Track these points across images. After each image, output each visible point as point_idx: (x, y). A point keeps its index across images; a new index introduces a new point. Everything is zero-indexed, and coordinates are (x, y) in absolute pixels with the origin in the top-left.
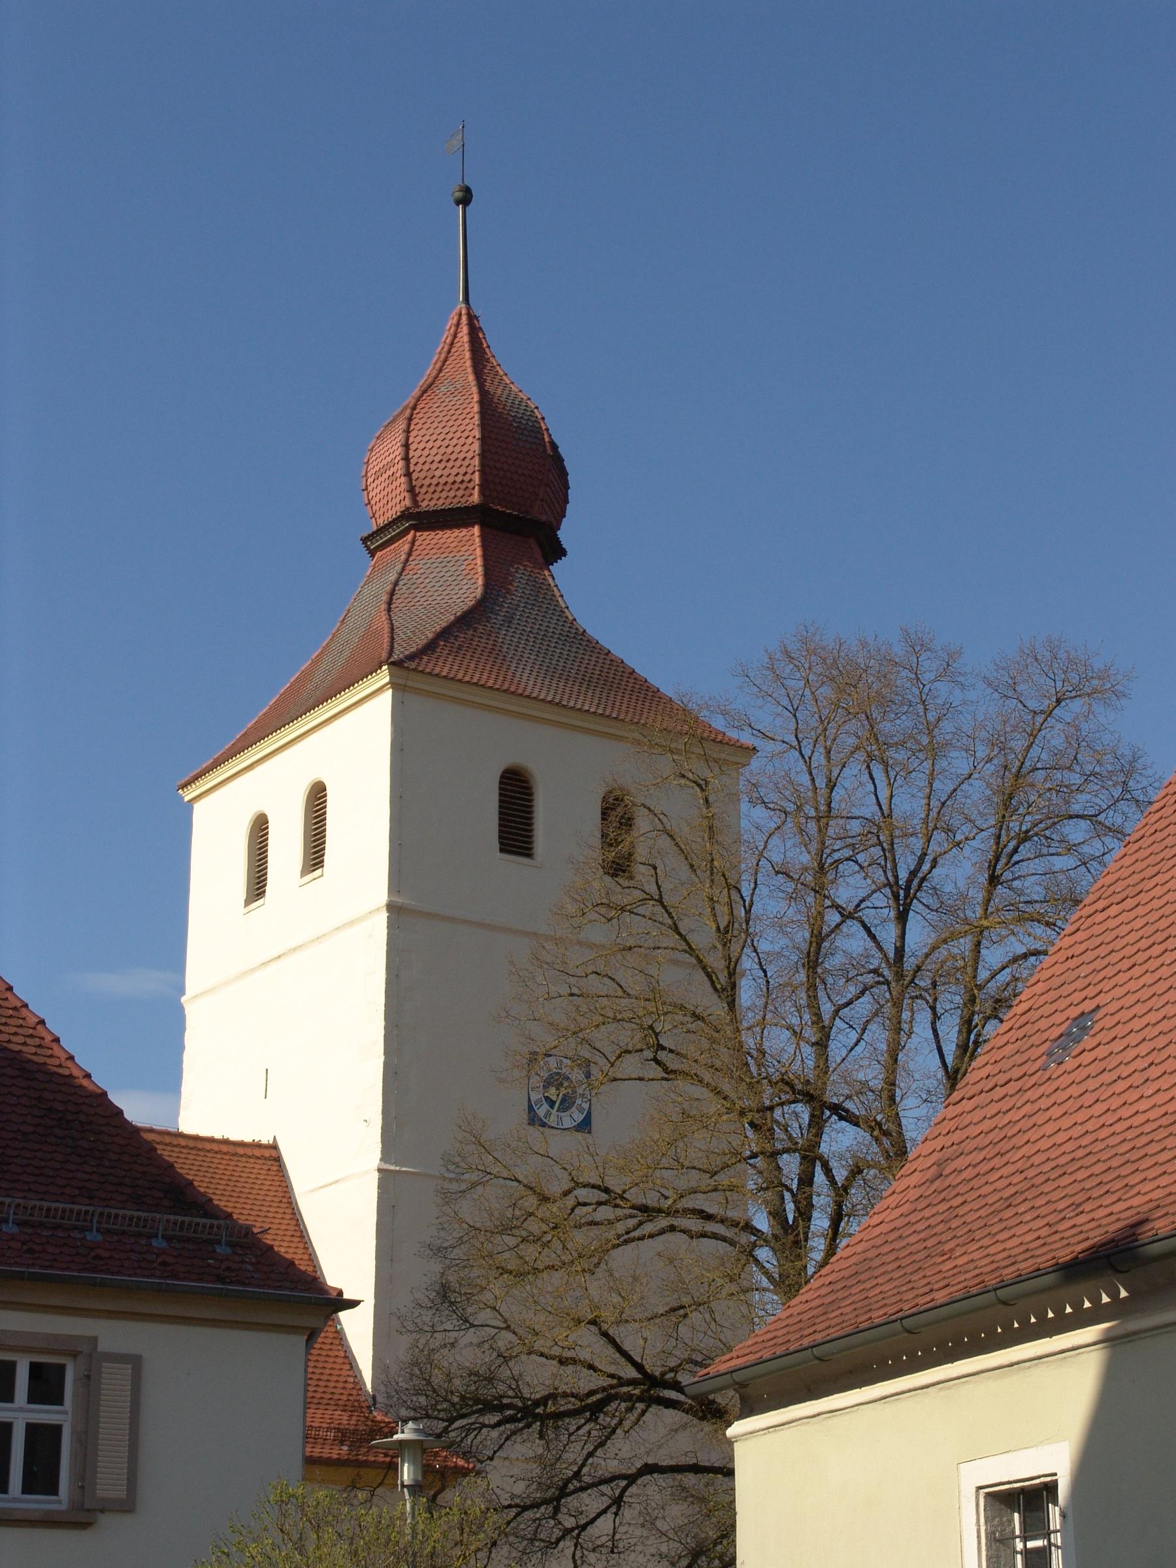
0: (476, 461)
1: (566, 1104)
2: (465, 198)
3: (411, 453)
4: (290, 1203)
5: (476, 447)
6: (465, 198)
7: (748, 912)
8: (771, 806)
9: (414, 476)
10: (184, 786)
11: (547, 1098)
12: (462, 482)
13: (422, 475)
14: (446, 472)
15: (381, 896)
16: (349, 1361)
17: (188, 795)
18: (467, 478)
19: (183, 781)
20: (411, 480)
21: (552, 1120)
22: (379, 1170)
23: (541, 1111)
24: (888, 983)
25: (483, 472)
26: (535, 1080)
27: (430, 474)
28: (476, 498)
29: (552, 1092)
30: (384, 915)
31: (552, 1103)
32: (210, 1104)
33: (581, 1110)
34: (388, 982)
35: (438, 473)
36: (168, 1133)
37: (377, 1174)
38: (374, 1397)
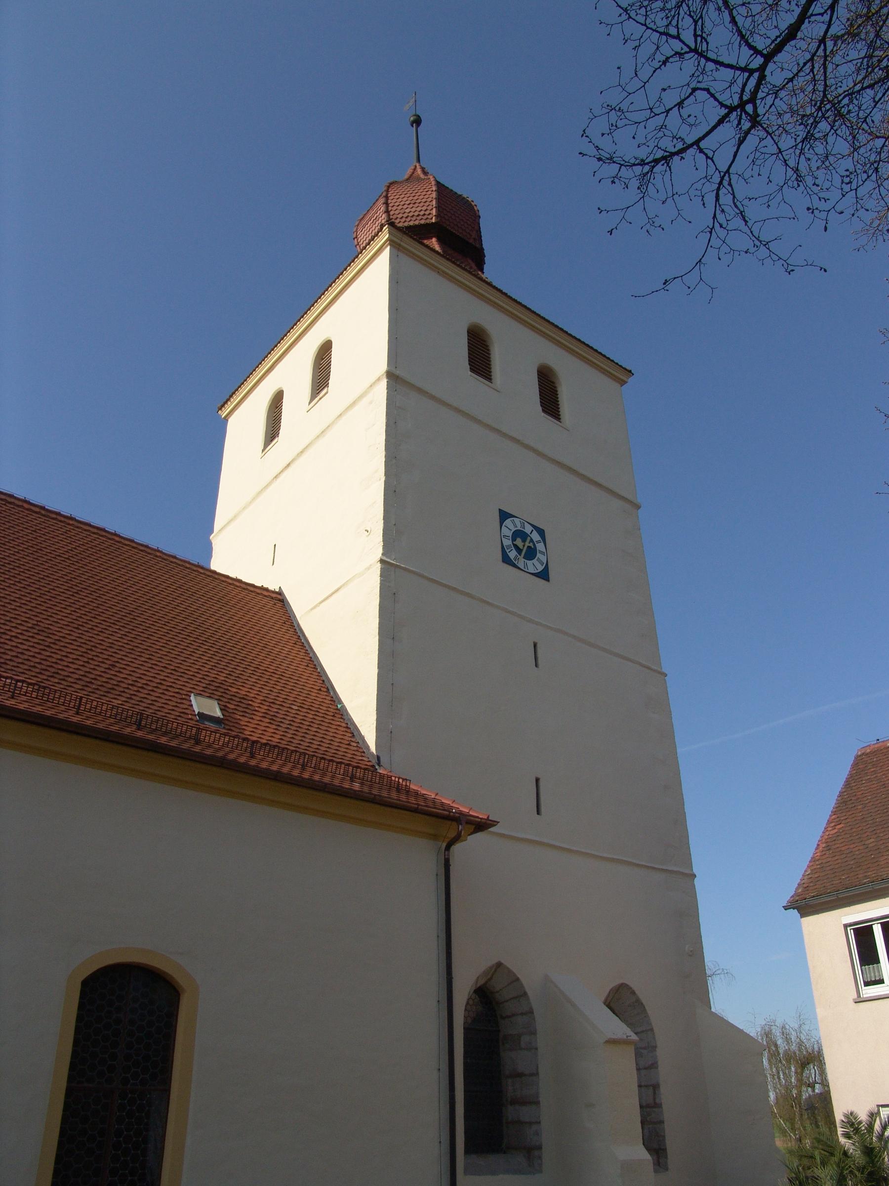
1: (531, 554)
2: (417, 122)
3: (389, 201)
4: (303, 645)
6: (417, 122)
9: (391, 213)
10: (220, 409)
14: (413, 210)
15: (381, 364)
17: (224, 413)
18: (427, 213)
19: (219, 405)
20: (389, 215)
21: (521, 563)
22: (382, 561)
23: (512, 554)
24: (832, 128)
25: (438, 208)
26: (505, 531)
27: (402, 211)
29: (519, 542)
30: (384, 382)
32: (237, 552)
34: (387, 425)
35: (407, 211)
36: (202, 568)
37: (379, 565)
38: (378, 758)
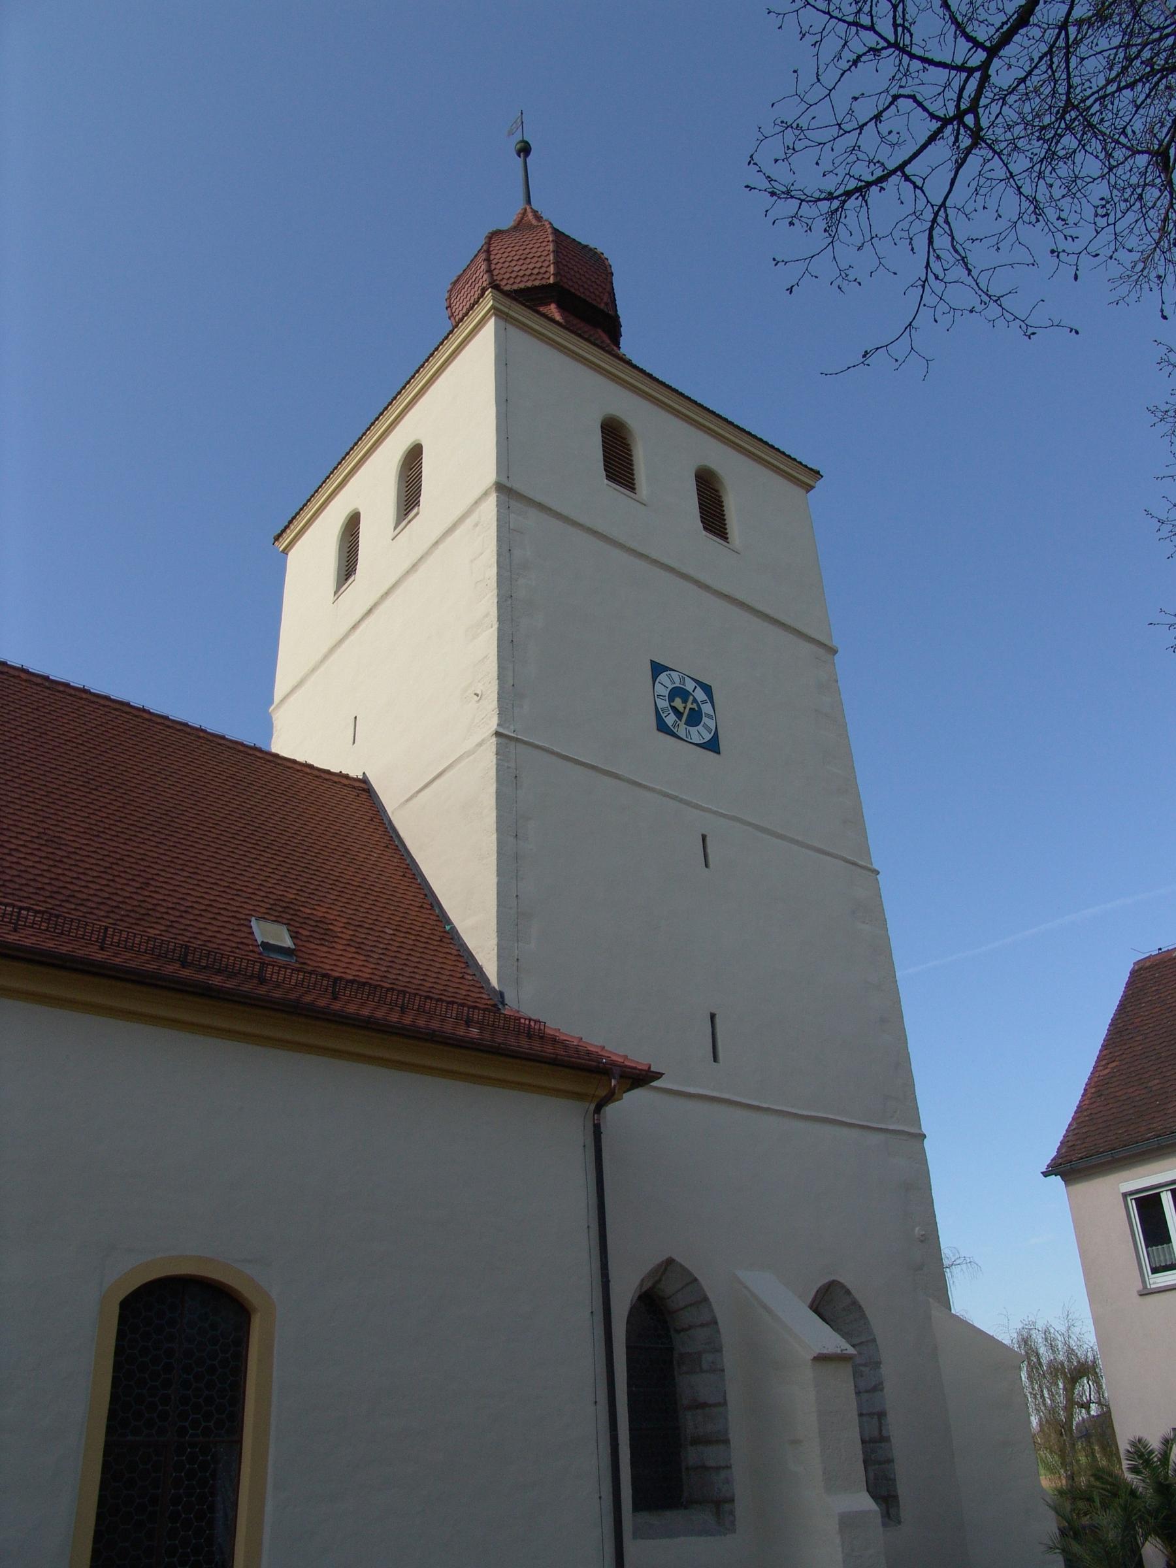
0: (551, 257)
5: (551, 247)
6: (525, 150)
7: (1050, 52)
8: (958, 247)
9: (495, 273)
10: (277, 538)
11: (675, 709)
12: (539, 273)
13: (502, 271)
16: (465, 958)
21: (682, 730)
23: (670, 719)
26: (659, 689)
28: (551, 281)
29: (678, 702)
31: (679, 714)
32: (304, 731)
33: (709, 730)
35: (516, 269)
36: (260, 750)
37: (494, 739)
